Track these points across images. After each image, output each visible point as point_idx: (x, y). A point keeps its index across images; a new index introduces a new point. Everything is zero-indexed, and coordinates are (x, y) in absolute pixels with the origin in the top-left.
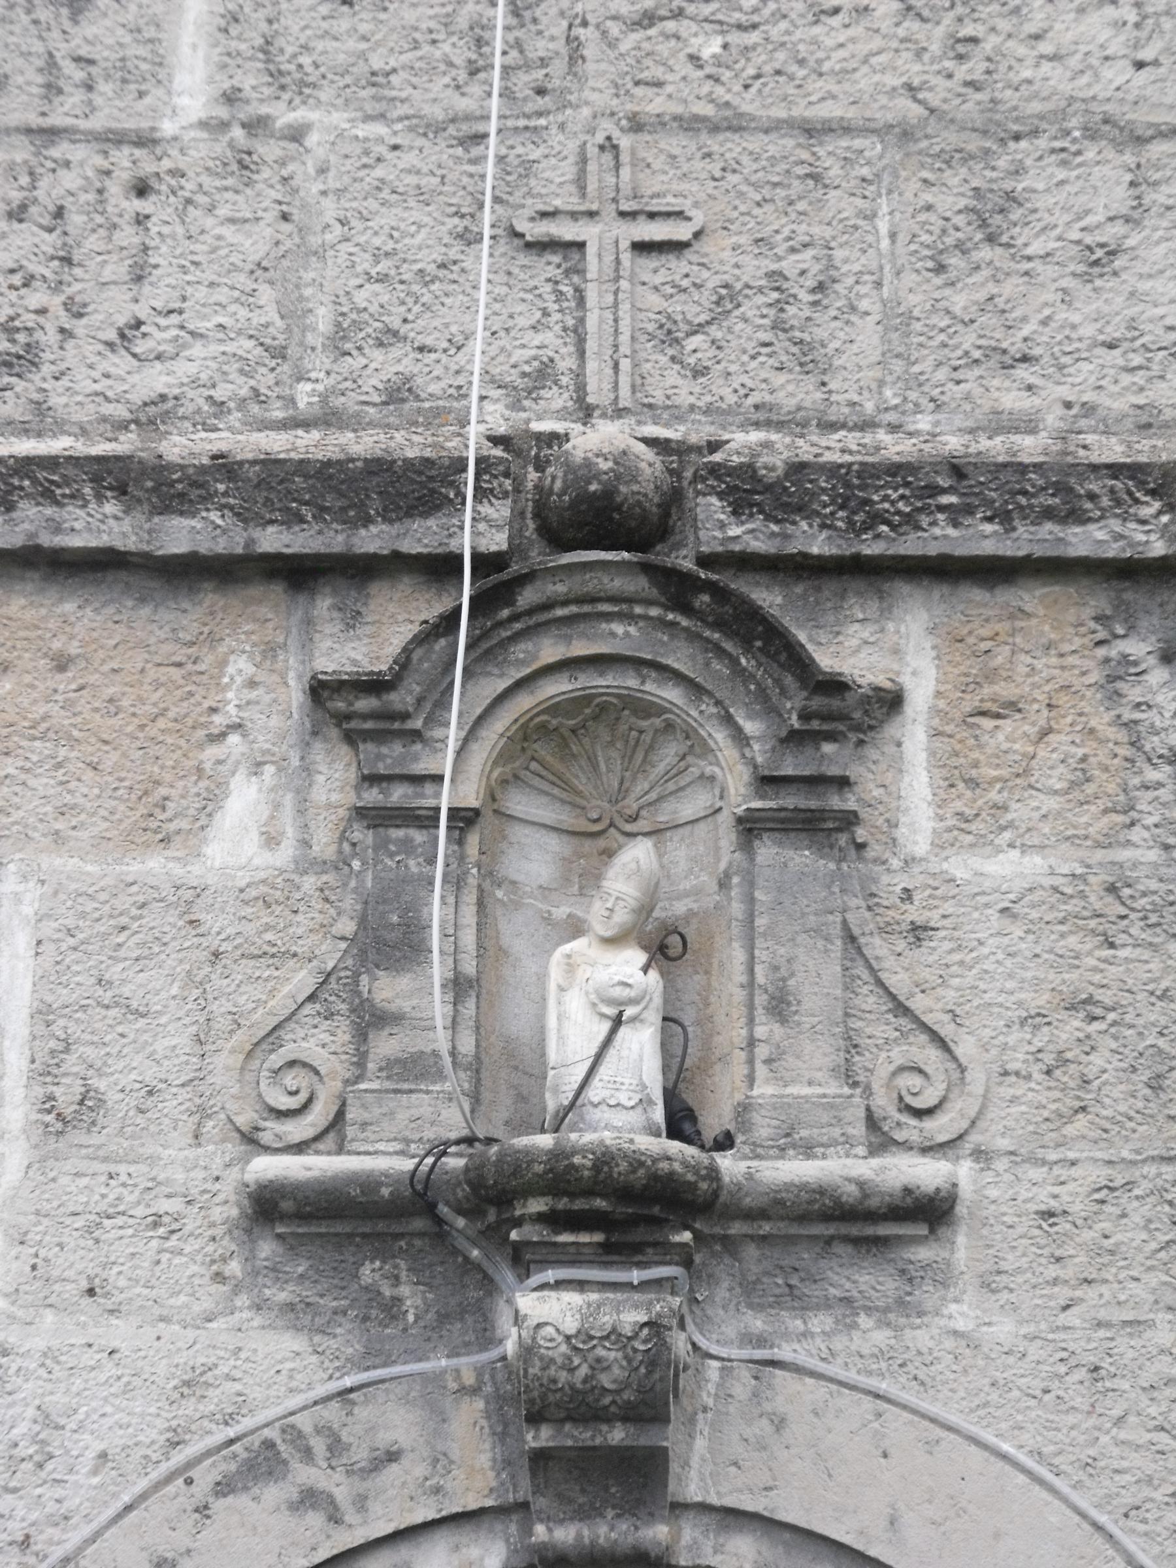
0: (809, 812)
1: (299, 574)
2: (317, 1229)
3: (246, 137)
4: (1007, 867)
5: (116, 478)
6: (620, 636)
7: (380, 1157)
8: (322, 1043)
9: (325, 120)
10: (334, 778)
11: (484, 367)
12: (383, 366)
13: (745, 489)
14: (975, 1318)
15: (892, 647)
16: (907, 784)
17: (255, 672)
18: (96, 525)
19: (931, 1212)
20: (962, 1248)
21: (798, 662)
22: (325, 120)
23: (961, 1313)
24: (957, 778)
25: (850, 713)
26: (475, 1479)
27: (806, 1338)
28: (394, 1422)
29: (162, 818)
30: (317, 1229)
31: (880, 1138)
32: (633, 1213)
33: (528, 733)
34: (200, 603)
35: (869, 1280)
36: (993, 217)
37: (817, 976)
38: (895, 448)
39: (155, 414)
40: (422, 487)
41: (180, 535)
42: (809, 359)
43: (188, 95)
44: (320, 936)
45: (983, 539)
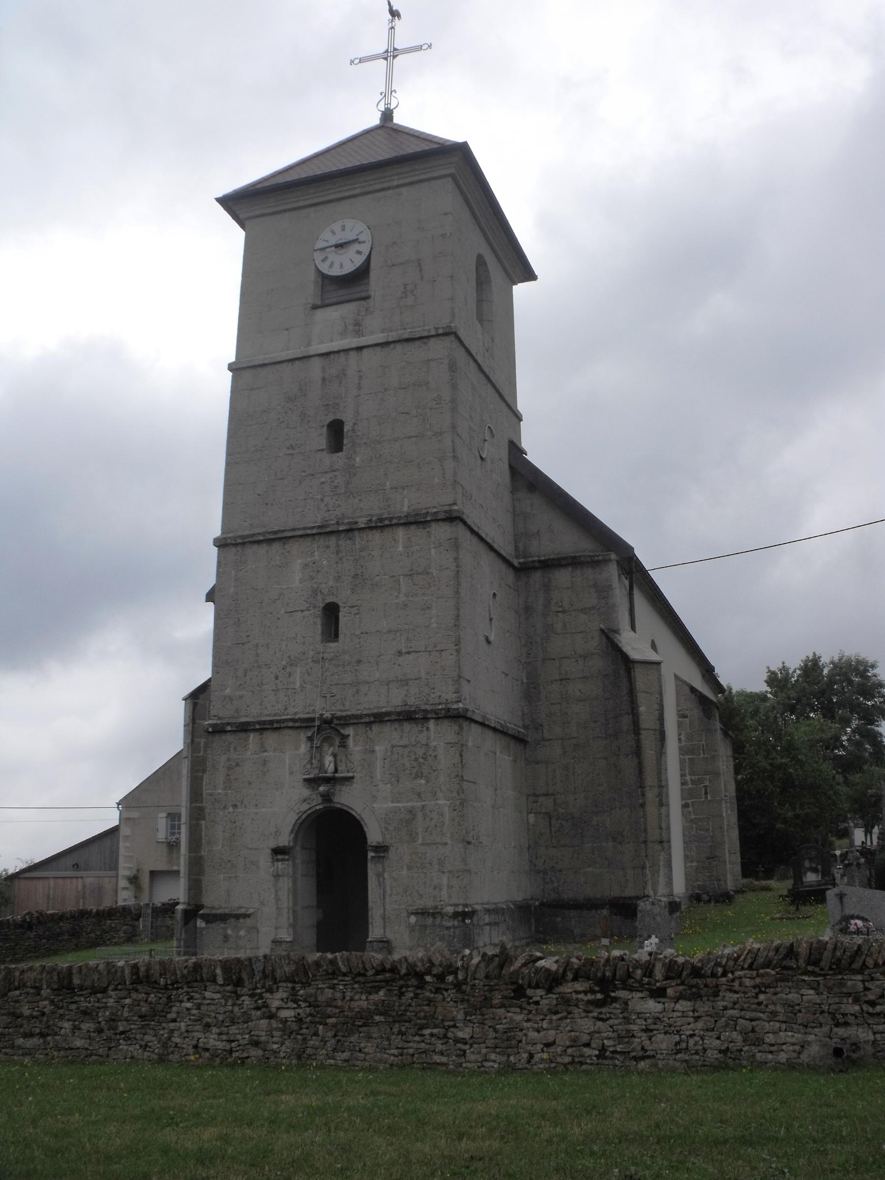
0: (343, 745)
1: (307, 727)
2: (308, 781)
3: (302, 688)
4: (358, 748)
5: (292, 720)
6: (328, 731)
7: (312, 776)
8: (308, 766)
9: (308, 686)
10: (309, 744)
11: (321, 708)
12: (312, 708)
13: (338, 718)
14: (356, 786)
15: (349, 731)
16: (351, 742)
17: (303, 735)
18: (291, 724)
19: (353, 778)
20: (355, 780)
21: (339, 732)
22: (308, 686)
23: (355, 785)
24: (354, 741)
25: (345, 737)
26: (320, 801)
27: (344, 788)
28: (314, 797)
29: (297, 748)
30: (308, 781)
31: (348, 772)
32: (328, 780)
33: (324, 738)
34: (458, 511)
35: (348, 783)
36: (358, 691)
37: (344, 758)
38: (349, 713)
39: (296, 714)
40: (312, 720)
41: (297, 725)
42: (344, 705)
43: (298, 685)
44: (308, 757)
45: (355, 721)
